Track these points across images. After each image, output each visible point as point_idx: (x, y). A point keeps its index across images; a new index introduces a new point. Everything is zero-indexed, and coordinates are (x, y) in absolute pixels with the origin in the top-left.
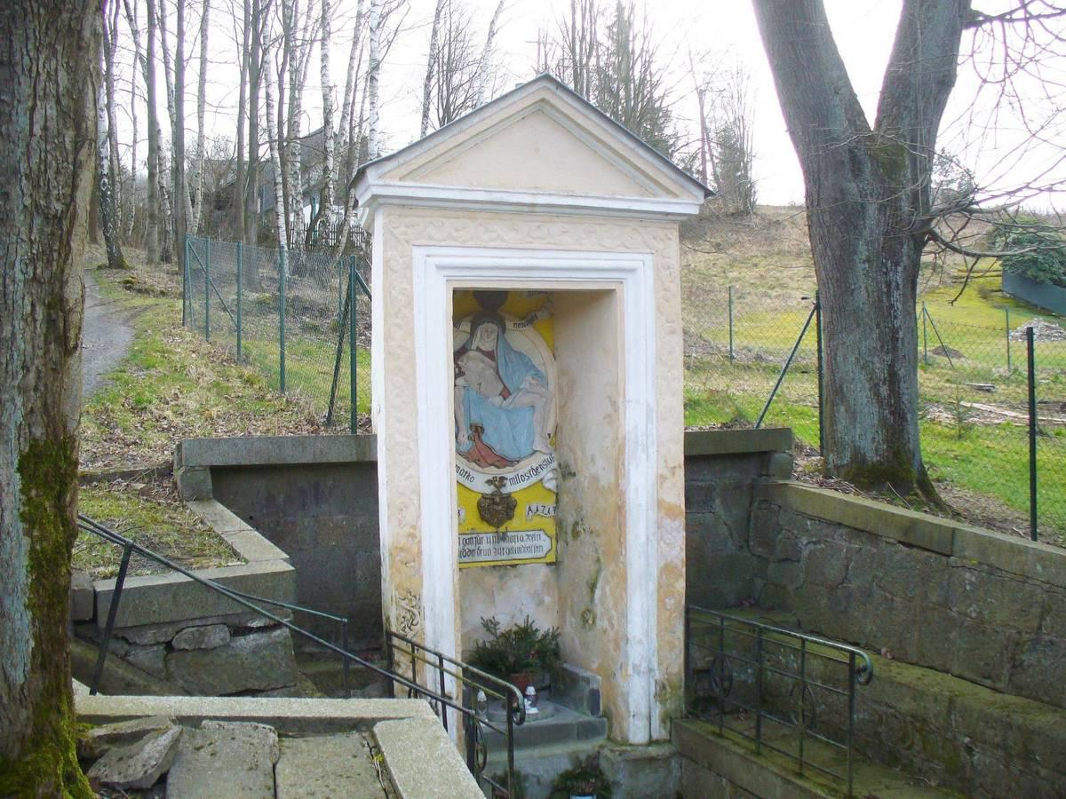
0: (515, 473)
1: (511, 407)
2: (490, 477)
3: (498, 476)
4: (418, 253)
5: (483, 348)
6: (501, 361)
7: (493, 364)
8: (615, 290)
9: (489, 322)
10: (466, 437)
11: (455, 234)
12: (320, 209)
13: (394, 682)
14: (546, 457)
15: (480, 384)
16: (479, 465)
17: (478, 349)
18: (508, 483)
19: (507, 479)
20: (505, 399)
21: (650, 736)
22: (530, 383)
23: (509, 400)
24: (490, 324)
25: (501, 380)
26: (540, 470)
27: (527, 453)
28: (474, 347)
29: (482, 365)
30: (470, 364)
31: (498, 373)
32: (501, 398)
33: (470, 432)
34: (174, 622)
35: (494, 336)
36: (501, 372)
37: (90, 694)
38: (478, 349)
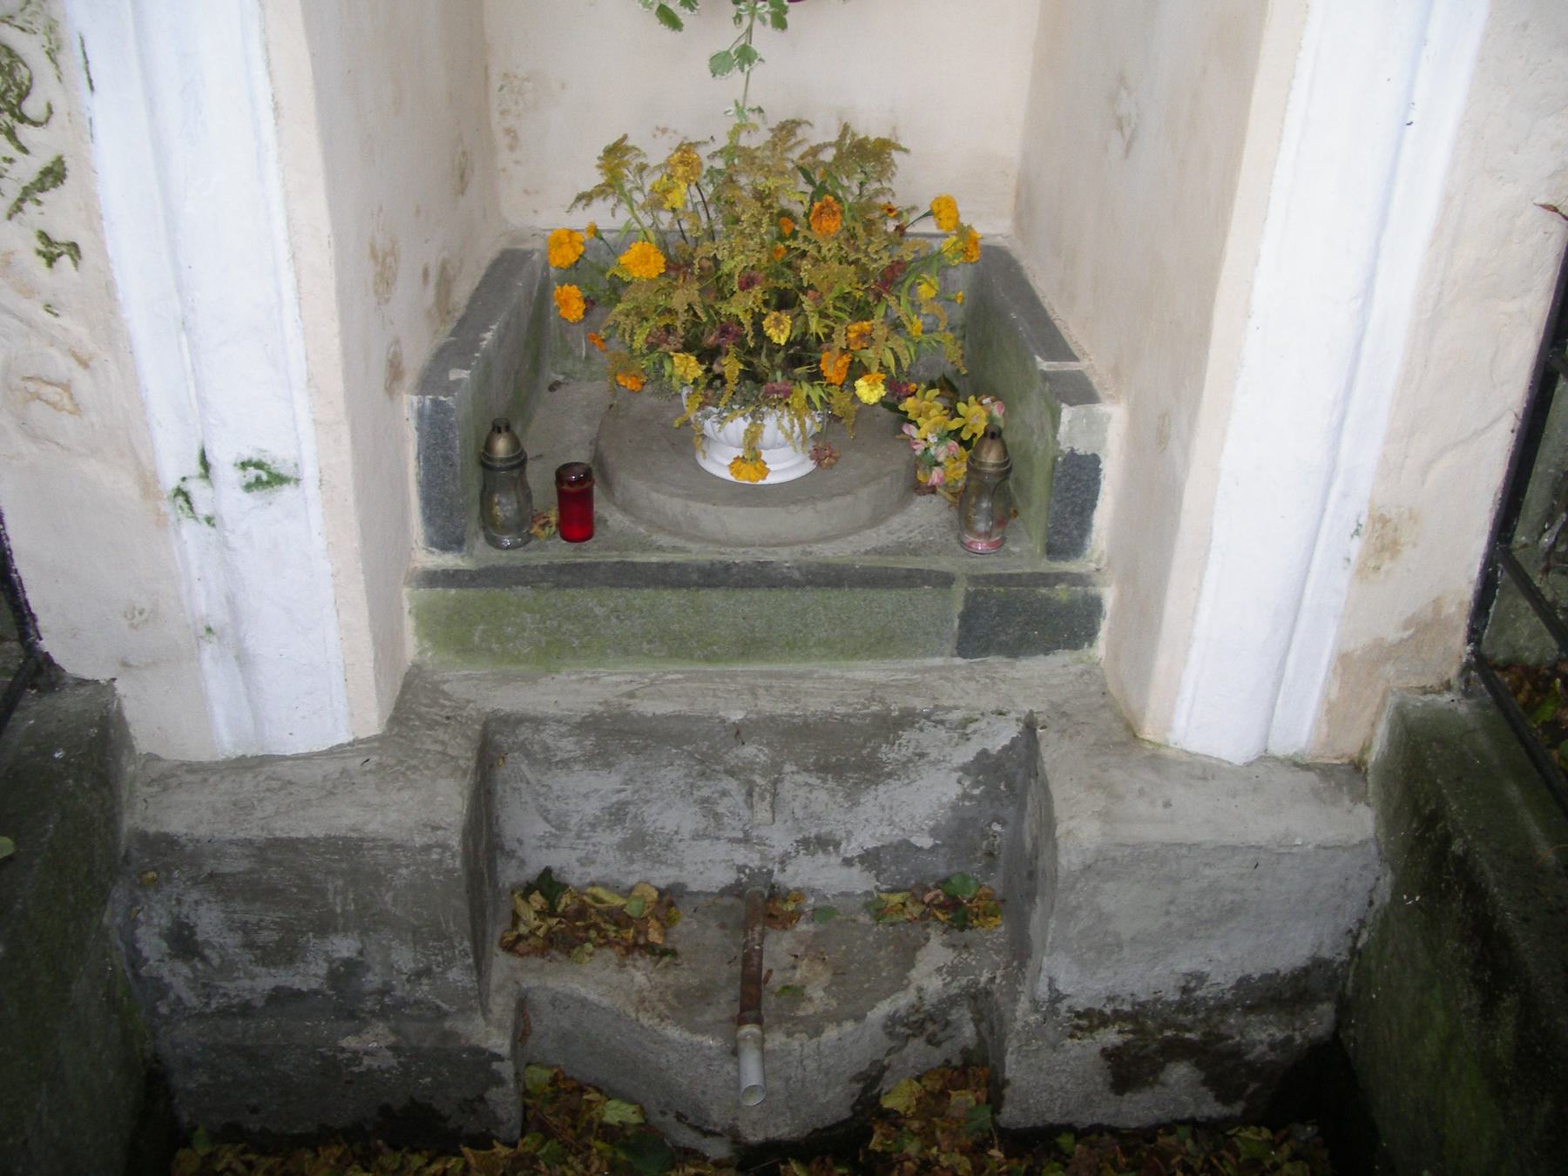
21: (1266, 737)
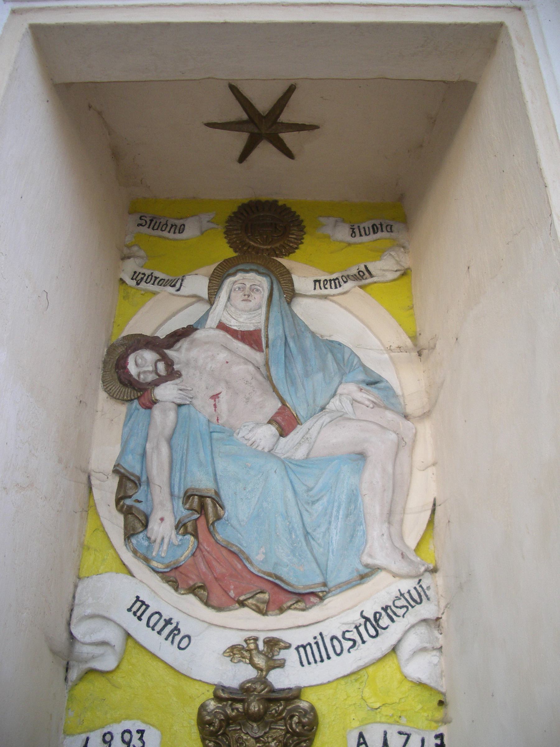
0: (314, 631)
1: (300, 454)
2: (238, 639)
3: (262, 637)
5: (234, 324)
6: (277, 351)
7: (258, 357)
8: (501, 25)
9: (247, 271)
10: (170, 522)
12: (151, 396)
13: (245, 602)
14: (407, 585)
15: (215, 397)
16: (207, 604)
17: (222, 326)
18: (291, 656)
19: (288, 647)
20: (283, 433)
22: (354, 401)
23: (295, 436)
24: (252, 275)
25: (275, 389)
26: (384, 621)
27: (344, 576)
28: (212, 321)
29: (223, 356)
30: (194, 353)
31: (269, 378)
32: (273, 430)
33: (183, 512)
34: (392, 502)
35: (261, 297)
36: (277, 373)
37: (140, 621)
38: (222, 326)
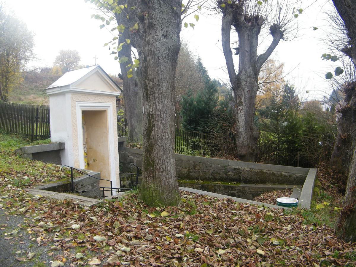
4: (77, 103)
11: (83, 99)
